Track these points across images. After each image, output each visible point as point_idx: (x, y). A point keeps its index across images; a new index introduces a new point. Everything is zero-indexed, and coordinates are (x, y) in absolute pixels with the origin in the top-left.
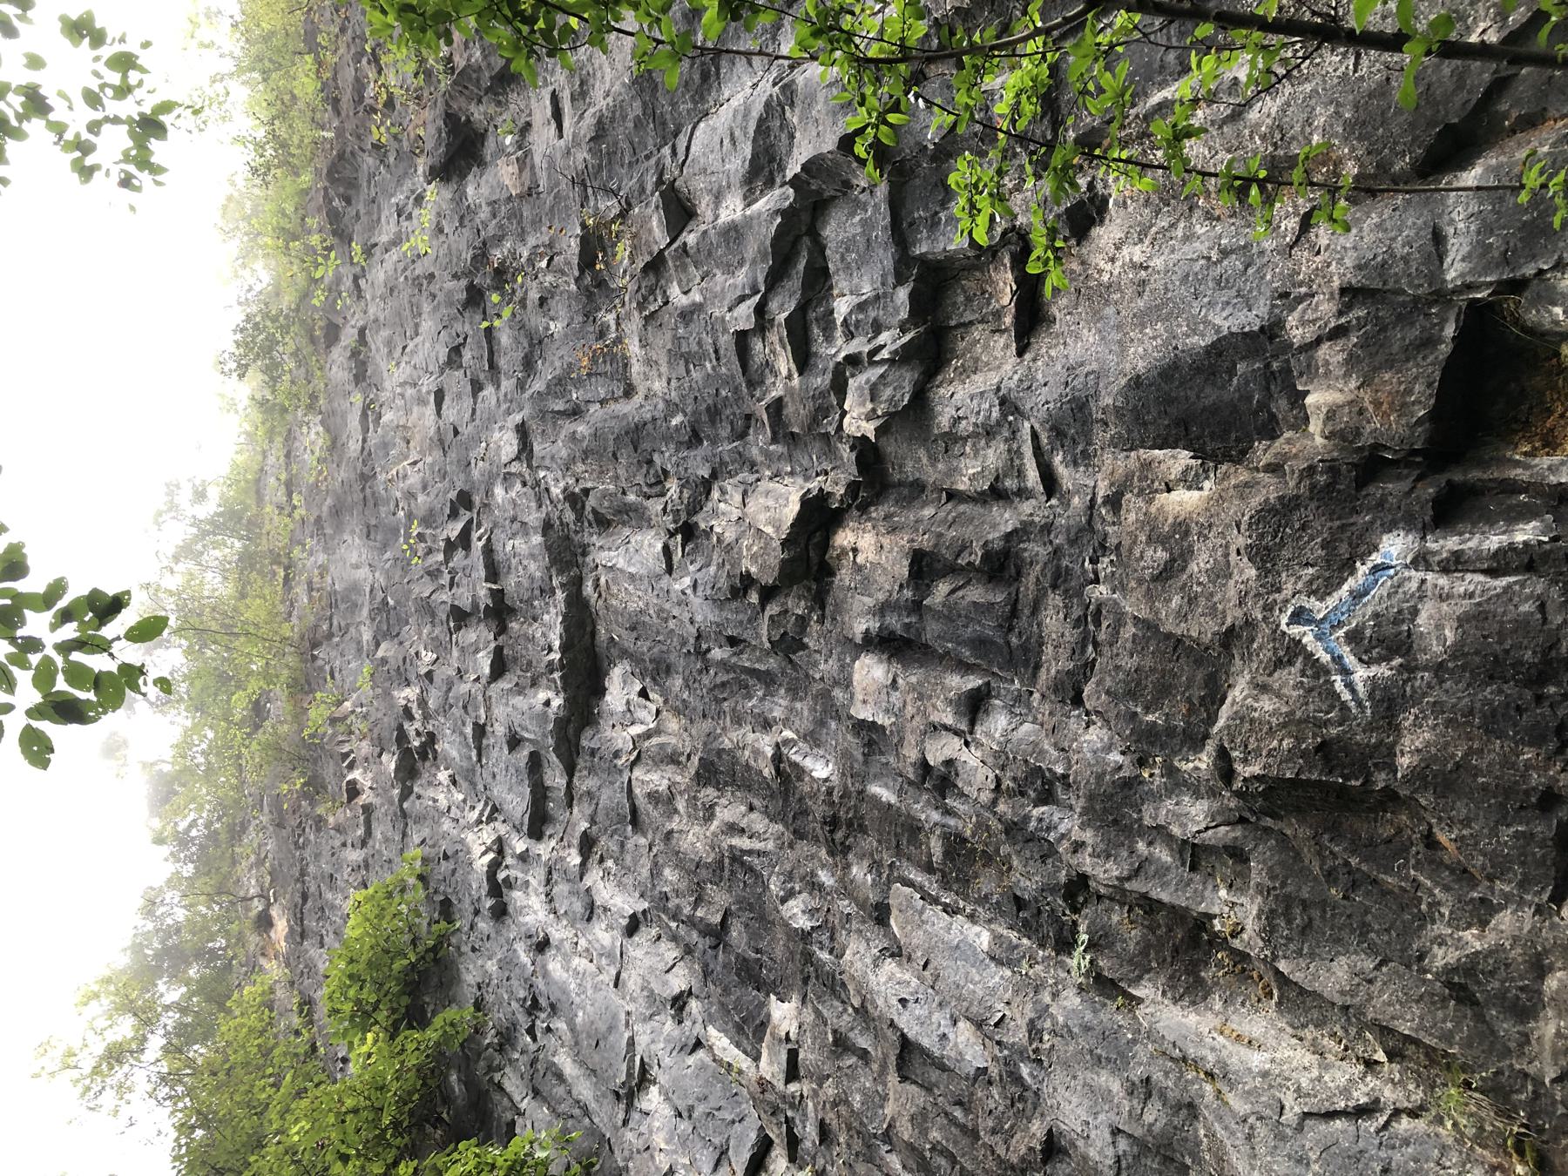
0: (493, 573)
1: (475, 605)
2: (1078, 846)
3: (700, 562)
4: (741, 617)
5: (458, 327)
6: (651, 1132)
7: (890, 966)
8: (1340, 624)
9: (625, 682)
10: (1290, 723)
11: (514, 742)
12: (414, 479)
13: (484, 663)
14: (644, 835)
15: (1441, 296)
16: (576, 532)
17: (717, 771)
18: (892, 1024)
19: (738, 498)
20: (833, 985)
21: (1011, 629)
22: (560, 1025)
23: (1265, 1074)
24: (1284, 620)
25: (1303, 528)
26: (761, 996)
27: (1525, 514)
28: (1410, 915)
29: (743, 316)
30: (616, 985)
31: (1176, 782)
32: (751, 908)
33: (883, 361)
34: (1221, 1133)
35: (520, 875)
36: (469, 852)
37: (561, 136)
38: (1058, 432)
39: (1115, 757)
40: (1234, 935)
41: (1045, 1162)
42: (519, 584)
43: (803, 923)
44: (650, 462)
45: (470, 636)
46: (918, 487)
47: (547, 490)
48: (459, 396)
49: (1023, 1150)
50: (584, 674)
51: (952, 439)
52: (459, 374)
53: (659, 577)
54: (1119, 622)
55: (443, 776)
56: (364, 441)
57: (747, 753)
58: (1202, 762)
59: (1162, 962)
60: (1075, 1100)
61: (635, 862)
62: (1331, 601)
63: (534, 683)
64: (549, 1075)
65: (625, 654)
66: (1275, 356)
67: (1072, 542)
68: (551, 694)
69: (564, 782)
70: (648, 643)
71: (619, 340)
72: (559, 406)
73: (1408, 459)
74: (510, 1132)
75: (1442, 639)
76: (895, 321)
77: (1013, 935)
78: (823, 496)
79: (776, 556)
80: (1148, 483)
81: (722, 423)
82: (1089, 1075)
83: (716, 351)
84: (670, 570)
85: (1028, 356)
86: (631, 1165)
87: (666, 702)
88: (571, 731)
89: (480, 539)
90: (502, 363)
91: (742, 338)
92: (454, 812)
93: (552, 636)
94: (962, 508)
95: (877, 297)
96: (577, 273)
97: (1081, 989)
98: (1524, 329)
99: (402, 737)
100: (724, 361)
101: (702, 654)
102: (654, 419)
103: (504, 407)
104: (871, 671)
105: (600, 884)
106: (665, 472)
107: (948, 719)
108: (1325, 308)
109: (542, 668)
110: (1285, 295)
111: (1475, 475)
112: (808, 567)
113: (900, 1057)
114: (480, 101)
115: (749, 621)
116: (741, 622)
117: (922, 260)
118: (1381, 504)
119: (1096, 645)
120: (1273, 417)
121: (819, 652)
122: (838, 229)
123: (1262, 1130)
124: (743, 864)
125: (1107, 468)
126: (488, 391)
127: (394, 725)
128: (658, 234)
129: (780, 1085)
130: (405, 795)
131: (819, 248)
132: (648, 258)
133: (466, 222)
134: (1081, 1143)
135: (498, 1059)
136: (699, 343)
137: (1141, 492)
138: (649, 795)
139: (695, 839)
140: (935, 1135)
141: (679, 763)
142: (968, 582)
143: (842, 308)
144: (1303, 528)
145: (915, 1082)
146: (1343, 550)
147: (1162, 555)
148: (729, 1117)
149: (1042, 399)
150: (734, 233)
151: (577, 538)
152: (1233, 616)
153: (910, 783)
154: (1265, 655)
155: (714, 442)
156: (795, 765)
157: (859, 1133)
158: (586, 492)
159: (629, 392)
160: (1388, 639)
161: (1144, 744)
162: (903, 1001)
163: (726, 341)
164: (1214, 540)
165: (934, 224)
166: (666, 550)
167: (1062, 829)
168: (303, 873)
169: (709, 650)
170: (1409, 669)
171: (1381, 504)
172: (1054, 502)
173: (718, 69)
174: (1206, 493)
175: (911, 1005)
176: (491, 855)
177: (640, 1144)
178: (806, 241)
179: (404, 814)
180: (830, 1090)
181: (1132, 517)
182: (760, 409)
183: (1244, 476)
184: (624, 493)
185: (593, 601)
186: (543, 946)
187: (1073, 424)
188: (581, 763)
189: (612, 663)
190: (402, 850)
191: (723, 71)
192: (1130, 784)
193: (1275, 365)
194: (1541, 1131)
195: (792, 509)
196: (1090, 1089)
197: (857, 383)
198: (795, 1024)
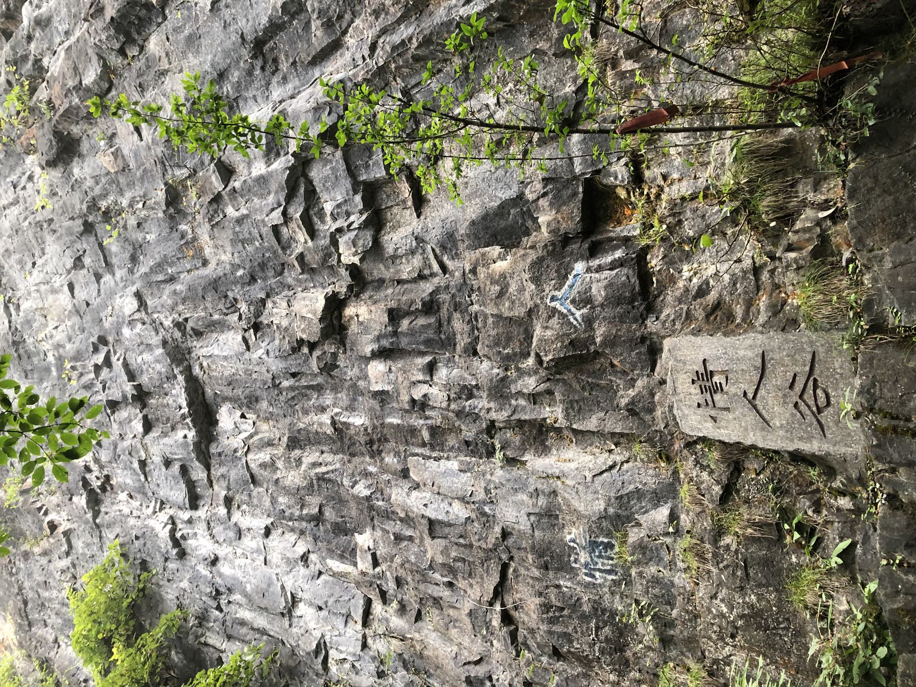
0: (131, 376)
1: (125, 397)
2: (489, 410)
3: (267, 340)
4: (298, 361)
5: (78, 246)
6: (306, 624)
7: (415, 494)
8: (568, 298)
9: (230, 413)
10: (558, 337)
11: (168, 463)
12: (60, 336)
13: (138, 426)
14: (261, 486)
15: (576, 178)
16: (183, 342)
17: (295, 442)
18: (423, 516)
19: (285, 304)
20: (388, 515)
21: (440, 332)
22: (236, 597)
23: (577, 469)
24: (548, 301)
25: (548, 267)
26: (348, 538)
27: (616, 248)
28: (611, 391)
29: (276, 217)
30: (265, 564)
31: (521, 373)
32: (333, 499)
33: (355, 229)
34: (567, 496)
35: (189, 531)
36: (153, 529)
37: (142, 140)
38: (443, 247)
39: (496, 371)
40: (555, 422)
41: (503, 541)
42: (151, 379)
43: (366, 492)
44: (226, 297)
45: (123, 414)
46: (381, 281)
47: (161, 324)
48: (87, 284)
49: (493, 540)
50: (203, 415)
51: (394, 258)
52: (85, 271)
53: (242, 354)
54: (486, 317)
55: (123, 496)
56: (10, 322)
57: (315, 426)
58: (531, 361)
59: (530, 445)
60: (510, 510)
61: (260, 500)
62: (563, 291)
63: (173, 428)
64: (235, 625)
65: (225, 399)
66: (524, 206)
67: (459, 291)
68: (186, 432)
69: (205, 475)
70: (241, 390)
71: (195, 239)
72: (161, 277)
73: (576, 236)
74: (220, 662)
75: (601, 295)
76: (357, 210)
77: (468, 459)
78: (335, 295)
79: (317, 328)
80: (485, 261)
81: (267, 269)
82: (513, 498)
83: (261, 236)
84: (248, 349)
85: (422, 217)
86: (300, 642)
87: (258, 416)
88: (203, 446)
89: (118, 360)
90: (114, 261)
91: (276, 229)
92: (135, 513)
93: (180, 400)
94: (405, 286)
95: (346, 201)
96: (164, 208)
97: (502, 467)
98: (603, 185)
99: (86, 483)
100: (265, 240)
101: (276, 386)
102: (225, 275)
103: (121, 285)
104: (377, 368)
105: (242, 519)
106: (235, 300)
107: (421, 377)
108: (538, 186)
109: (178, 418)
110: (522, 182)
111: (599, 237)
112: (334, 329)
113: (430, 529)
114: (77, 123)
115: (304, 362)
116: (299, 364)
117: (364, 183)
118: (572, 253)
119: (478, 329)
120: (527, 228)
121: (347, 367)
122: (317, 173)
123: (580, 488)
124: (324, 480)
125: (468, 258)
126: (107, 278)
127: (78, 478)
128: (216, 183)
129: (371, 572)
130: (95, 516)
131: (309, 182)
132: (212, 196)
133: (75, 189)
134: (516, 526)
135: (200, 631)
136: (250, 233)
137: (484, 265)
138: (260, 465)
139: (293, 478)
140: (454, 554)
141: (273, 445)
142: (416, 317)
143: (328, 207)
144: (548, 267)
145: (439, 537)
146: (563, 271)
147: (498, 288)
148: (347, 598)
149: (434, 235)
150: (262, 180)
151: (183, 346)
152: (530, 304)
153: (407, 411)
154: (544, 315)
155: (265, 279)
156: (345, 423)
157: (417, 571)
158: (186, 320)
159: (205, 263)
160: (584, 300)
161: (506, 362)
162: (425, 505)
163: (266, 231)
164: (516, 278)
165: (367, 166)
166: (245, 340)
167: (480, 406)
168: (20, 589)
169: (280, 383)
170: (593, 308)
171: (572, 253)
172: (447, 276)
173: (237, 104)
174: (509, 261)
175: (429, 505)
176: (169, 527)
177: (302, 631)
178: (302, 180)
179: (98, 526)
180: (398, 560)
181: (482, 276)
182: (292, 259)
183: (522, 252)
184: (211, 315)
185: (200, 376)
186: (215, 561)
187: (449, 243)
188: (213, 462)
189: (218, 406)
190: (101, 546)
191: (241, 105)
192: (506, 377)
193: (525, 209)
194: (665, 447)
195: (321, 303)
196: (515, 503)
197: (343, 241)
198: (372, 541)
